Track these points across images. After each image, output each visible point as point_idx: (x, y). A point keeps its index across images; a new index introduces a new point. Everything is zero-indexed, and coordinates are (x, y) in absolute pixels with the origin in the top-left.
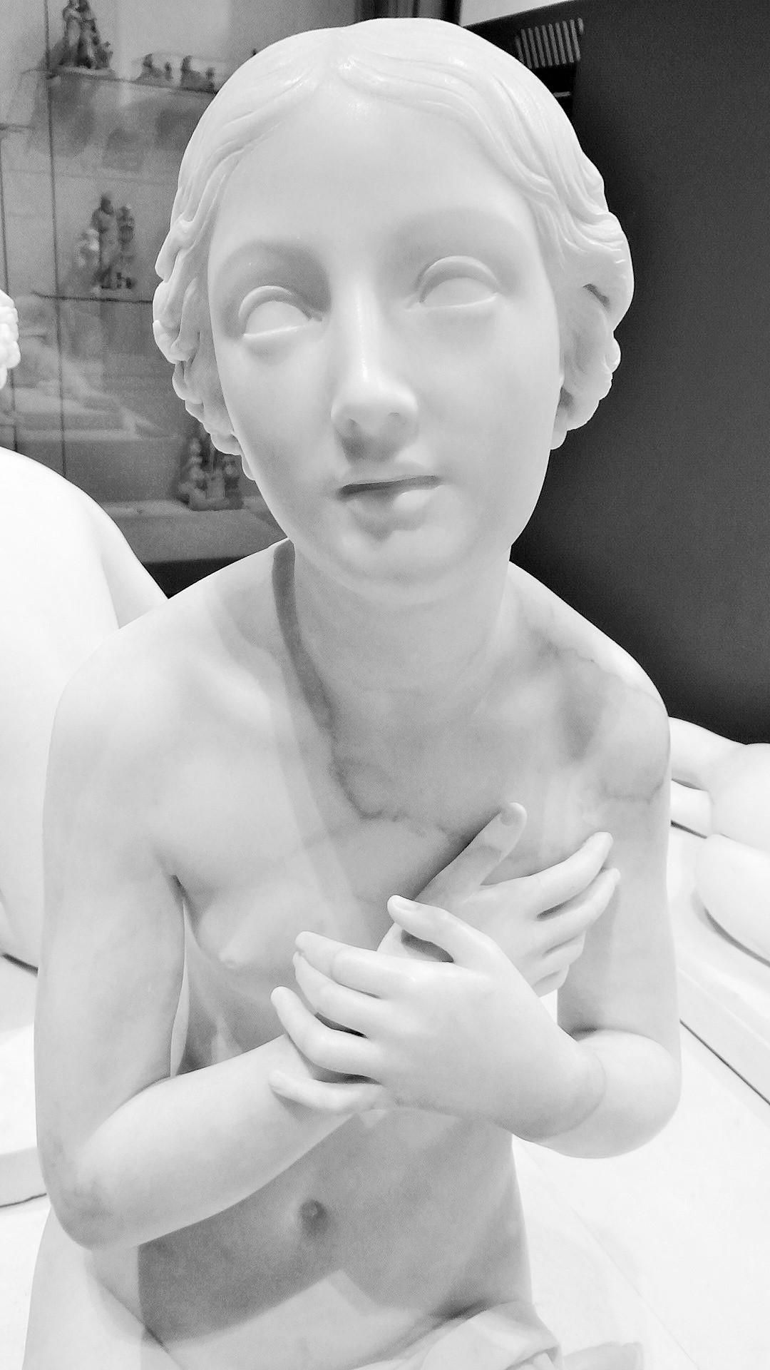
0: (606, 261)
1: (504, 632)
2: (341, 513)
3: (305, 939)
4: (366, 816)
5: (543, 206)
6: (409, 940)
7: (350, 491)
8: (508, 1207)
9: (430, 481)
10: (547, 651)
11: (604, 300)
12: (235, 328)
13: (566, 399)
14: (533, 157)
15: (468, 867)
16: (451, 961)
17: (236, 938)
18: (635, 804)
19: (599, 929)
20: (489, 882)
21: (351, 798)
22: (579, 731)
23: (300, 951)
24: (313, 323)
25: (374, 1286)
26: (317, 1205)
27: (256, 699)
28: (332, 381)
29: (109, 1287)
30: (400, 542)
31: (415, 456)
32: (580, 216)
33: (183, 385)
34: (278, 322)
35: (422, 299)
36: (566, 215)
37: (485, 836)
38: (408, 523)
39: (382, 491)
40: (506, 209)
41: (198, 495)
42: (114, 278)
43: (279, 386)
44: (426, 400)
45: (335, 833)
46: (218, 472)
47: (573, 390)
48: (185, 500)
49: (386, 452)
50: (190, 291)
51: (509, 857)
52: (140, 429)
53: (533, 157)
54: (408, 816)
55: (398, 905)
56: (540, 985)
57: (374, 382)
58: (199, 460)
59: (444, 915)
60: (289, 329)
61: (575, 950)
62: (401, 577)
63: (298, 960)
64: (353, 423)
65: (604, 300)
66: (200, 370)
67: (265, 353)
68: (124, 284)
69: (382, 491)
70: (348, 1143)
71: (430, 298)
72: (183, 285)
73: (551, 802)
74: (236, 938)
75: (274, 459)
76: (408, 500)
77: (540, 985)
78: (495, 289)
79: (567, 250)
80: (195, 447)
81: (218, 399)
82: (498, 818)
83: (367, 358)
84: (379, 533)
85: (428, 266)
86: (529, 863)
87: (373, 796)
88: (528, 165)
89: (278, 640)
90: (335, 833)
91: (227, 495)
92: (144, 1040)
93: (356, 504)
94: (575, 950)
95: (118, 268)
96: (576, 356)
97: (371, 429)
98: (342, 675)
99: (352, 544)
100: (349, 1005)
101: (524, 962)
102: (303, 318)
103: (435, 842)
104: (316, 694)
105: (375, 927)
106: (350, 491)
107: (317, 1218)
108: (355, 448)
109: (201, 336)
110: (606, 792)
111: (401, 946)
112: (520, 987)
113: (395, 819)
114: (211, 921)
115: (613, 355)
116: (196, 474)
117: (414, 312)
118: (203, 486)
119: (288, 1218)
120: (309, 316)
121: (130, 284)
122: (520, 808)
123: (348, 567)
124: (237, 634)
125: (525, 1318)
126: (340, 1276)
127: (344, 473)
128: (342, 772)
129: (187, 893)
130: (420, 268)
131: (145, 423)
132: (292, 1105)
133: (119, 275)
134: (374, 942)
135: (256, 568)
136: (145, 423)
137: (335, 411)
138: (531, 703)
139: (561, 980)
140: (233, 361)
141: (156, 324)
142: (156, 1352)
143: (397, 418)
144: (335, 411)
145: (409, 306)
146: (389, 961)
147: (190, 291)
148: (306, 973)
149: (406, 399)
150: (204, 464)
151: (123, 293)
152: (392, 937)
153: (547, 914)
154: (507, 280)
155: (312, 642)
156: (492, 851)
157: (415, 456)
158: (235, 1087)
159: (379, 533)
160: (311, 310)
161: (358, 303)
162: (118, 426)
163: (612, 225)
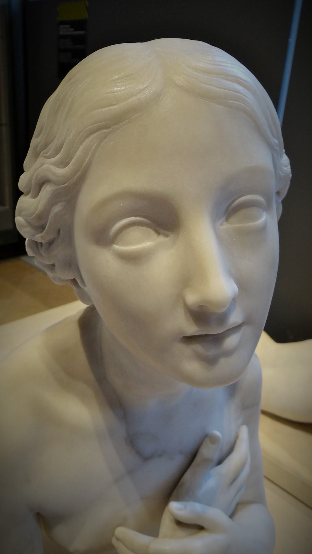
3: (120, 531)
4: (146, 459)
6: (180, 523)
7: (189, 339)
16: (201, 528)
21: (138, 453)
23: (118, 539)
24: (161, 239)
28: (190, 274)
34: (140, 240)
38: (229, 353)
39: (217, 339)
49: (222, 318)
59: (198, 507)
60: (147, 244)
63: (114, 541)
66: (59, 252)
67: (132, 259)
71: (233, 219)
76: (231, 341)
82: (207, 441)
84: (210, 362)
85: (233, 202)
88: (273, 135)
89: (91, 376)
93: (198, 347)
99: (193, 367)
102: (155, 235)
104: (114, 402)
109: (61, 231)
111: (176, 527)
113: (160, 456)
120: (158, 233)
122: (217, 433)
127: (192, 329)
128: (132, 441)
145: (221, 225)
147: (57, 209)
156: (207, 461)
159: (210, 362)
160: (161, 231)
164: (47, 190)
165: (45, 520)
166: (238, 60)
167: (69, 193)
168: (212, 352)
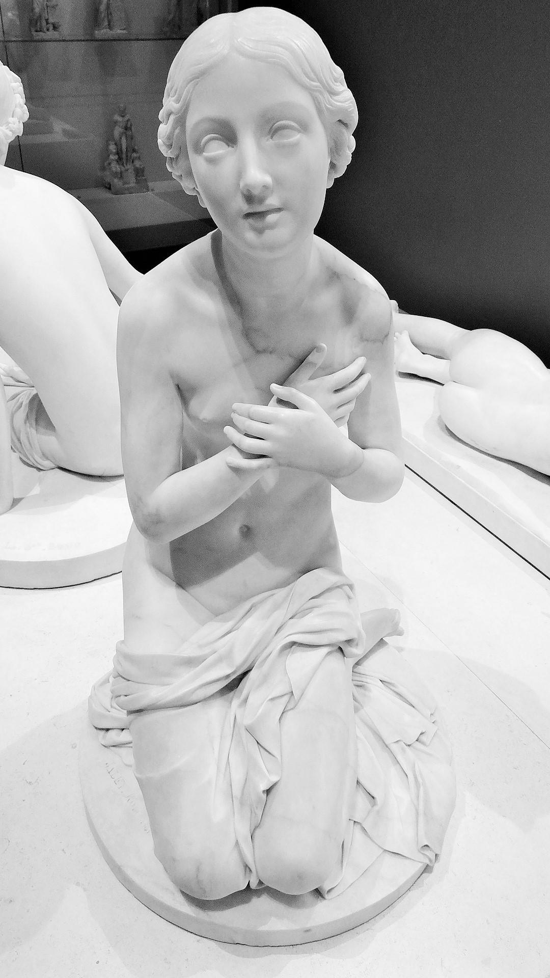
0: (345, 111)
1: (313, 267)
2: (245, 224)
3: (236, 406)
4: (258, 352)
5: (317, 94)
7: (248, 215)
8: (330, 531)
9: (279, 210)
10: (334, 276)
11: (346, 125)
12: (199, 150)
13: (333, 166)
14: (312, 75)
15: (304, 374)
17: (206, 408)
18: (377, 341)
19: (362, 399)
20: (311, 379)
21: (252, 345)
22: (349, 311)
23: (234, 411)
24: (230, 148)
25: (273, 558)
26: (246, 526)
27: (209, 303)
28: (240, 173)
29: (159, 569)
30: (269, 235)
31: (273, 201)
32: (333, 93)
33: (172, 167)
34: (217, 149)
35: (272, 137)
36: (327, 95)
37: (310, 358)
38: (272, 227)
39: (261, 215)
40: (301, 100)
41: (116, 182)
42: (44, 23)
43: (219, 173)
44: (278, 181)
45: (246, 360)
46: (129, 166)
47: (335, 162)
48: (109, 187)
49: (261, 201)
50: (177, 131)
51: (320, 367)
52: (65, 132)
53: (312, 75)
54: (278, 354)
55: (275, 387)
56: (338, 420)
57: (257, 175)
58: (116, 157)
59: (294, 390)
60: (221, 152)
61: (351, 406)
62: (271, 248)
63: (233, 415)
64: (248, 190)
65: (346, 125)
66: (181, 162)
67: (212, 161)
68: (51, 28)
69: (261, 215)
70: (256, 500)
72: (174, 128)
73: (337, 343)
74: (206, 408)
75: (219, 203)
76: (271, 218)
77: (338, 420)
78: (299, 132)
79: (327, 109)
80: (112, 148)
81: (190, 174)
83: (251, 164)
84: (260, 231)
86: (328, 369)
87: (261, 344)
90: (246, 360)
91: (138, 182)
92: (171, 454)
93: (251, 221)
94: (351, 406)
95: (45, 15)
96: (335, 149)
97: (256, 192)
98: (246, 288)
99: (250, 236)
100: (257, 427)
101: (329, 410)
103: (289, 362)
104: (234, 299)
105: (266, 397)
106: (248, 215)
107: (247, 532)
108: (249, 198)
110: (363, 338)
112: (328, 420)
113: (271, 353)
114: (194, 404)
115: (352, 142)
116: (115, 167)
117: (269, 142)
118: (120, 176)
119: (234, 531)
121: (55, 28)
123: (251, 246)
124: (199, 274)
125: (338, 572)
126: (258, 554)
127: (246, 208)
129: (184, 392)
130: (272, 126)
131: (68, 127)
132: (236, 470)
133: (47, 20)
134: (266, 404)
135: (203, 243)
136: (68, 127)
137: (242, 185)
138: (327, 300)
139: (347, 419)
140: (198, 163)
141: (159, 141)
142: (181, 591)
143: (265, 187)
144: (242, 185)
146: (272, 410)
147: (177, 131)
148: (236, 418)
149: (268, 179)
150: (120, 160)
151: (51, 34)
152: (273, 400)
153: (337, 391)
154: (304, 128)
155: (232, 277)
156: (313, 364)
157: (273, 201)
158: (208, 470)
159: (260, 231)
161: (248, 142)
162: (50, 131)
163: (349, 94)
164: (172, 117)
165: (174, 860)
166: (174, 224)
167: (181, 121)
168: (259, 224)
